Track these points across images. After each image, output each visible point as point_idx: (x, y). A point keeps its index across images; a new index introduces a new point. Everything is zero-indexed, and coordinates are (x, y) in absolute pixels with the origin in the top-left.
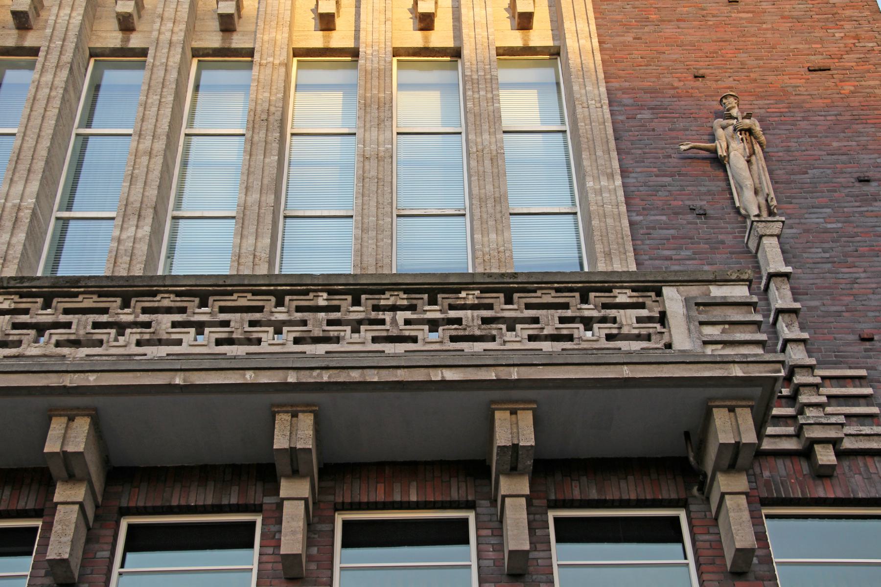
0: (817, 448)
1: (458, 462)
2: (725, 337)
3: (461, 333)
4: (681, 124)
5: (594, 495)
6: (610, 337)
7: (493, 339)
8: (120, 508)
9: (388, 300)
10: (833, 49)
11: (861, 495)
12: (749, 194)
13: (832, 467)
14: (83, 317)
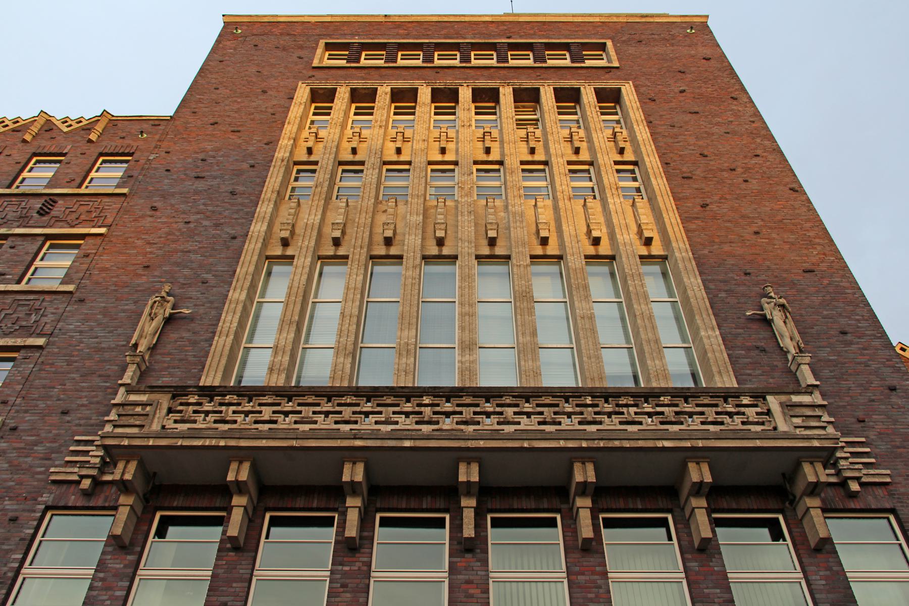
2: (805, 424)
4: (742, 300)
5: (734, 506)
6: (743, 423)
7: (682, 423)
9: (623, 401)
10: (814, 260)
11: (873, 507)
13: (858, 492)
14: (468, 409)
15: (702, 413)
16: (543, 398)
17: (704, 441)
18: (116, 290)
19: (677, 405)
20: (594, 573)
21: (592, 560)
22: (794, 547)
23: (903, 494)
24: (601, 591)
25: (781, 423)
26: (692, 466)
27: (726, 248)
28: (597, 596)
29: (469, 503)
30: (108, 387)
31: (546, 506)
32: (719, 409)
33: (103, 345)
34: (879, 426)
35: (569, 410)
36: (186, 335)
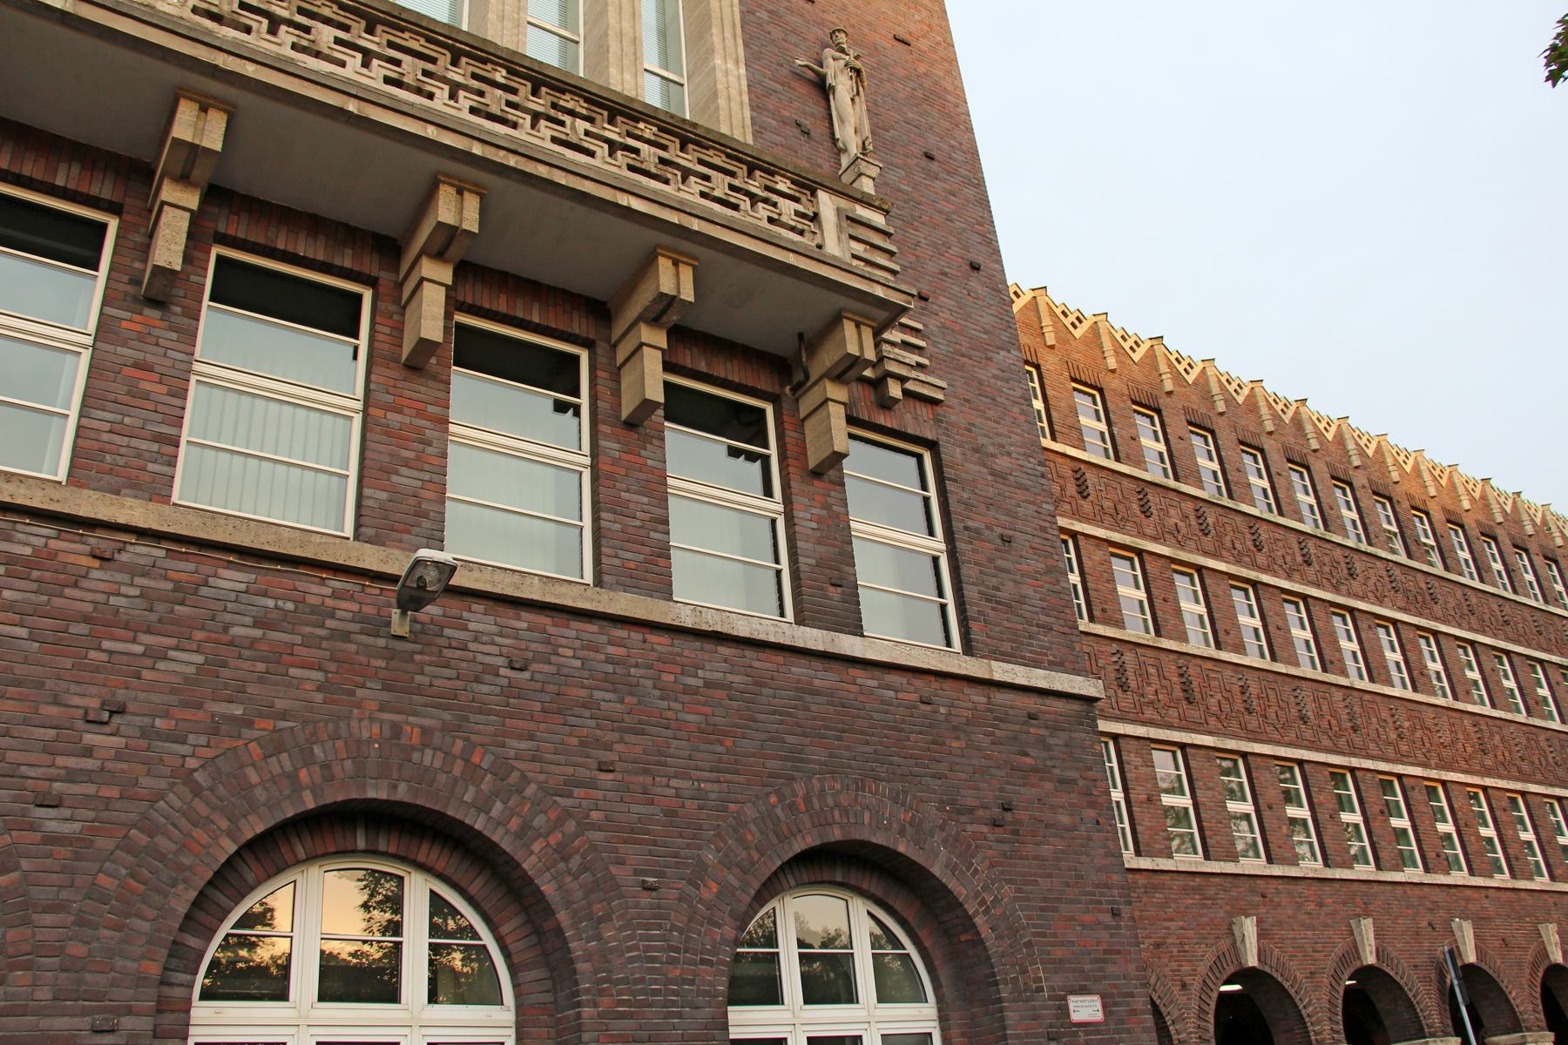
0: (890, 381)
1: (580, 296)
3: (638, 165)
4: (793, 38)
5: (702, 367)
8: (216, 233)
9: (568, 102)
10: (913, 28)
11: (910, 431)
12: (850, 130)
13: (897, 401)
15: (707, 178)
16: (406, 35)
17: (703, 223)
19: (664, 148)
20: (421, 414)
21: (421, 390)
22: (780, 462)
23: (953, 425)
24: (429, 450)
26: (664, 264)
28: (418, 458)
29: (178, 204)
31: (348, 264)
32: (736, 183)
34: (945, 315)
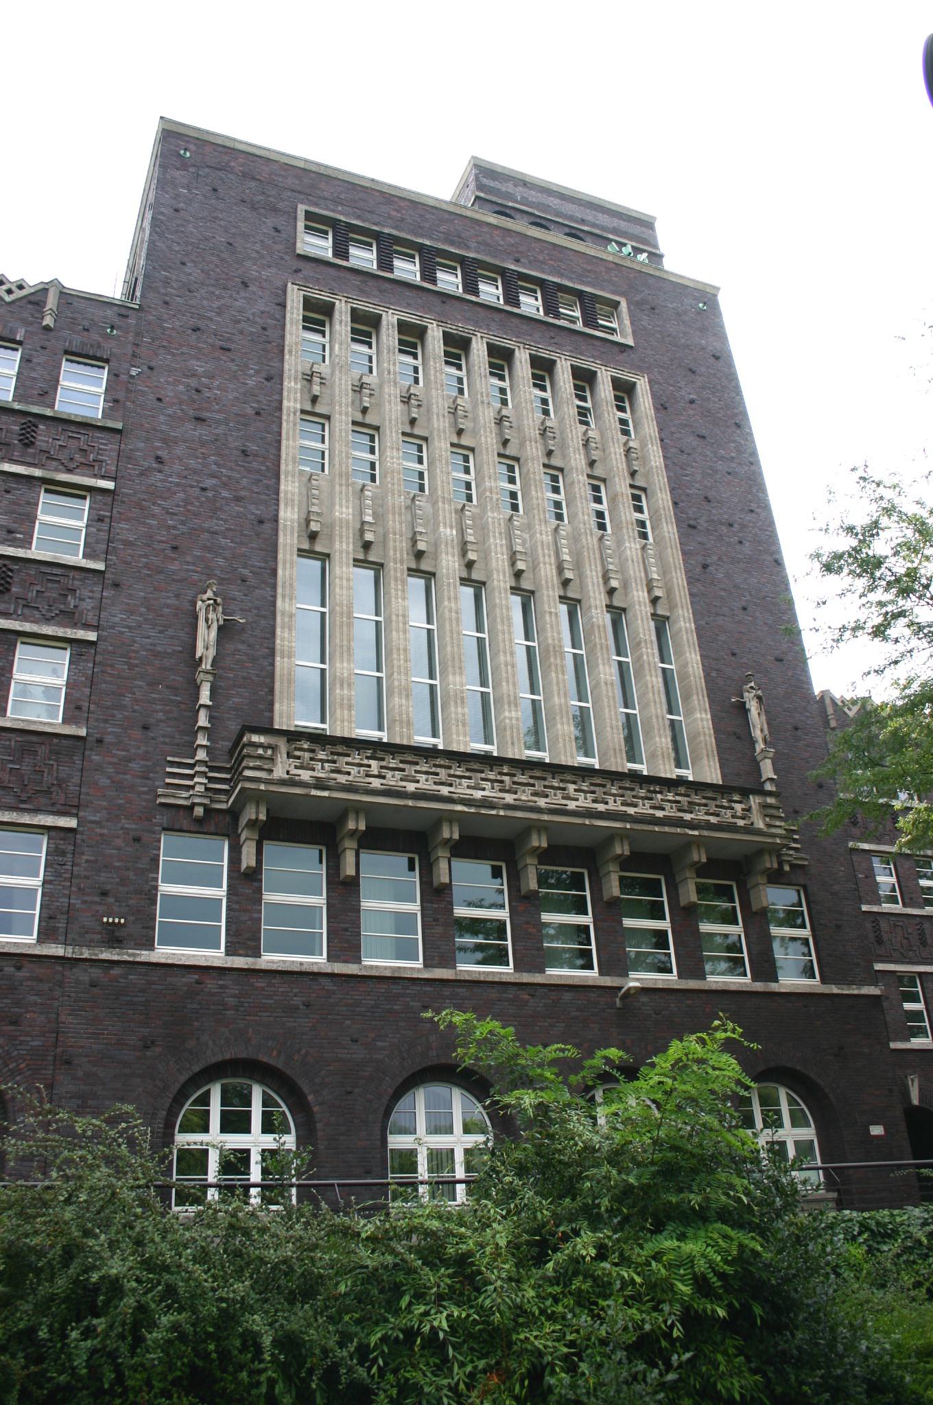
18: (150, 576)
25: (752, 815)
27: (720, 620)
30: (180, 702)
33: (159, 649)
35: (614, 791)
36: (241, 647)
